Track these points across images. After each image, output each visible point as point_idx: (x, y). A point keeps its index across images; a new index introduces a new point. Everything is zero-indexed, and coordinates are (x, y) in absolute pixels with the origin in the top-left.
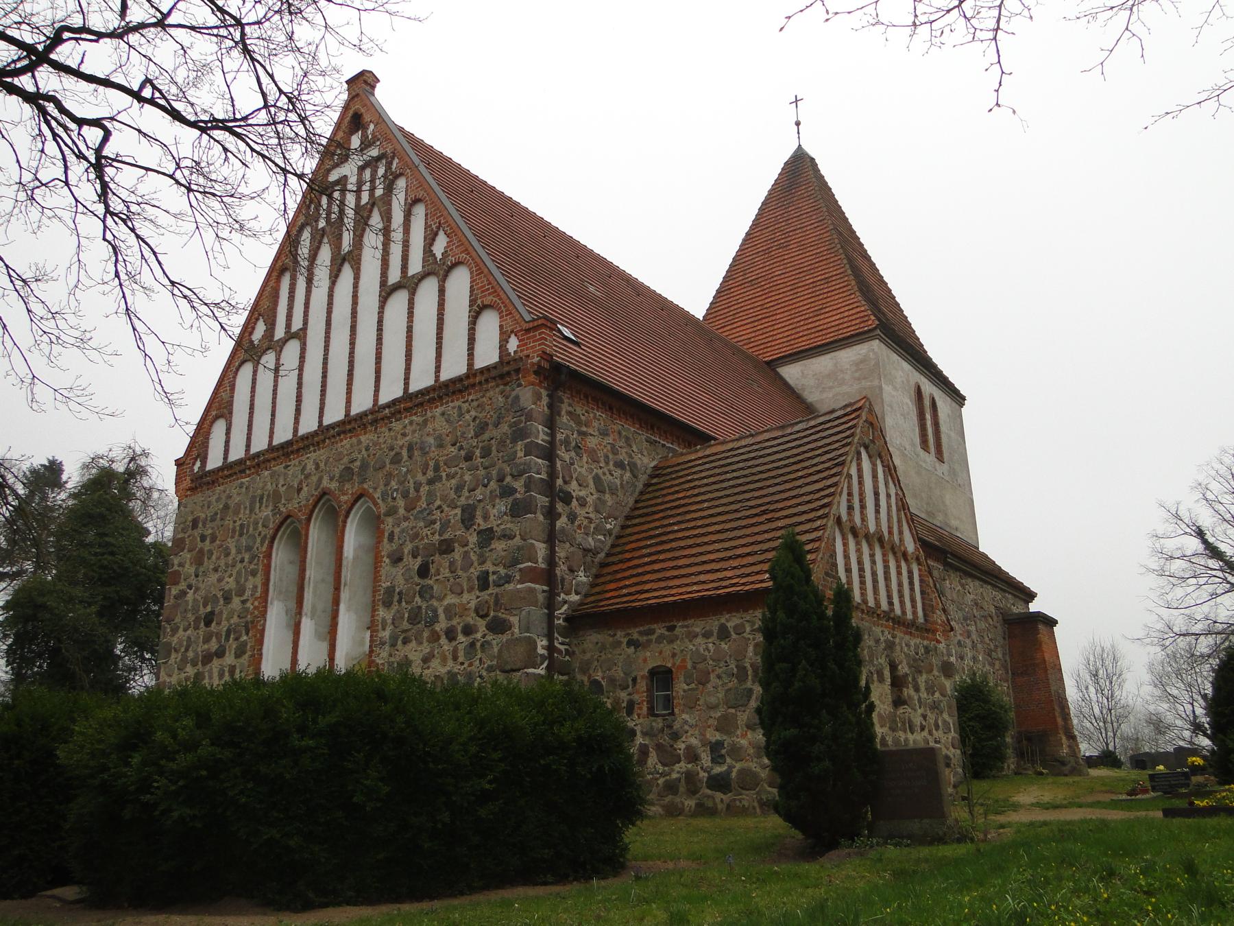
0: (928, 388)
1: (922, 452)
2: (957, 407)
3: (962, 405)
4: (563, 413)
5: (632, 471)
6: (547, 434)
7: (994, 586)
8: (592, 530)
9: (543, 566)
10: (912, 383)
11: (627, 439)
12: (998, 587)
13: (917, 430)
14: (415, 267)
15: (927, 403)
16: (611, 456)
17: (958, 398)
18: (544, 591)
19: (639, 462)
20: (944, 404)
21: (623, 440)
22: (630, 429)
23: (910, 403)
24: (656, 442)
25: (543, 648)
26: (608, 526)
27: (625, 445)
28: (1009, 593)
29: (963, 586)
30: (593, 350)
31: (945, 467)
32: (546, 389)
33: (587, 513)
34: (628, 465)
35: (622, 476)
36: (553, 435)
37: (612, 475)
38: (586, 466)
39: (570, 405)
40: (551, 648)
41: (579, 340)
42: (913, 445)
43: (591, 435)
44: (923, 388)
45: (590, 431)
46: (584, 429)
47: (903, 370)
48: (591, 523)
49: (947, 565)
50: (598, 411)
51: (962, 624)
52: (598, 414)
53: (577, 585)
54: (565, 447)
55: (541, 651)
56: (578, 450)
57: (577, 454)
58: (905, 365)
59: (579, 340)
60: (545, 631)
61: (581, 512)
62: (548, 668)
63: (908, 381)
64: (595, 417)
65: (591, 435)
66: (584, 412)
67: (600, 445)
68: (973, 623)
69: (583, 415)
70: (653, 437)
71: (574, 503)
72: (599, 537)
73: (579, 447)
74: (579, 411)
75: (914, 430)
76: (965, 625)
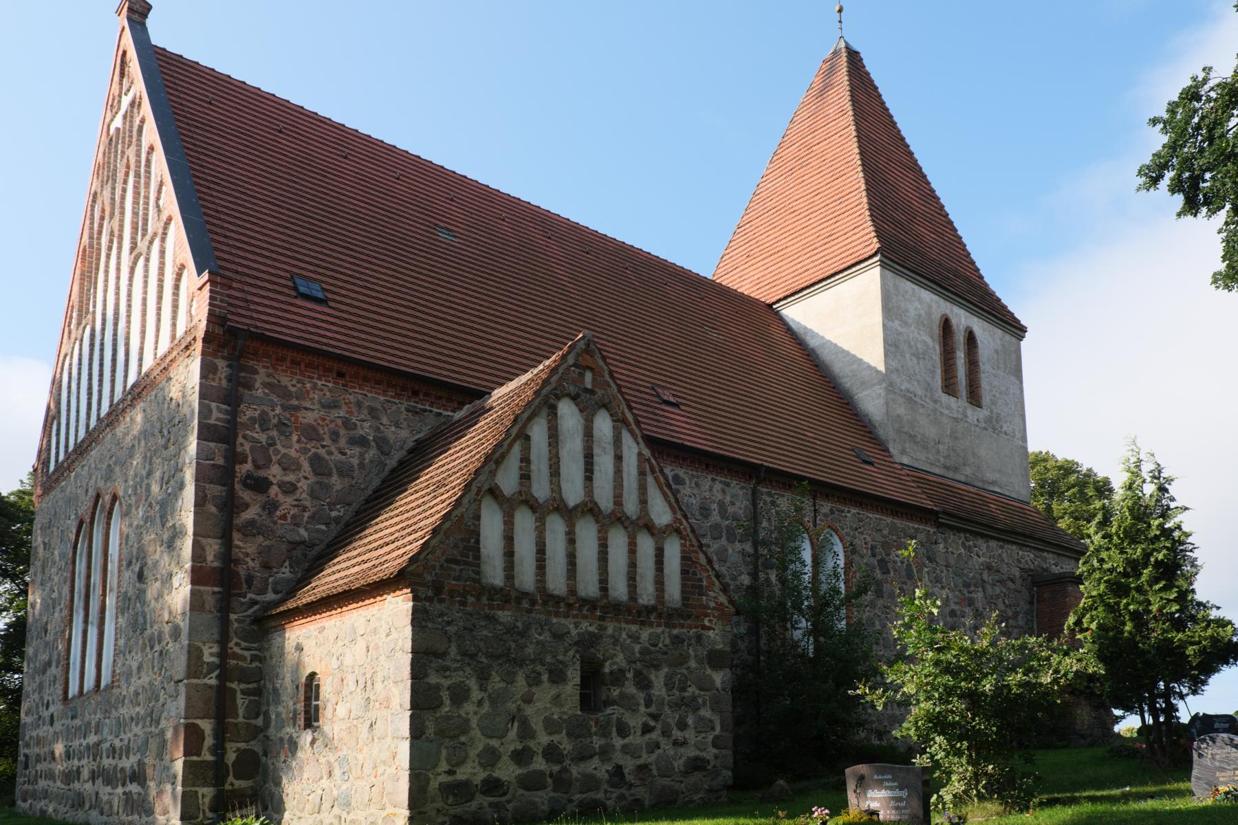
0: (962, 319)
1: (945, 398)
2: (1014, 340)
3: (1021, 338)
4: (257, 385)
5: (379, 448)
6: (226, 412)
7: (1021, 546)
8: (305, 519)
9: (216, 564)
10: (936, 317)
11: (372, 411)
12: (1027, 546)
13: (939, 372)
14: (290, 284)
15: (960, 338)
16: (342, 432)
17: (1017, 330)
18: (214, 593)
19: (391, 438)
20: (988, 336)
21: (366, 412)
22: (376, 398)
23: (929, 340)
24: (425, 411)
25: (211, 654)
26: (334, 514)
27: (368, 417)
28: (1048, 552)
29: (969, 549)
30: (729, 412)
31: (982, 413)
32: (223, 358)
33: (296, 500)
34: (374, 440)
35: (362, 455)
36: (234, 414)
37: (345, 454)
38: (297, 446)
39: (269, 376)
40: (223, 654)
41: (679, 400)
42: (928, 388)
43: (306, 409)
44: (954, 321)
45: (308, 404)
46: (294, 402)
47: (920, 300)
48: (304, 511)
49: (939, 525)
50: (319, 379)
51: (960, 591)
52: (319, 383)
53: (275, 583)
54: (260, 426)
55: (207, 658)
56: (283, 428)
57: (281, 433)
58: (926, 295)
59: (679, 400)
60: (216, 637)
61: (287, 502)
62: (218, 677)
63: (929, 314)
64: (315, 387)
65: (306, 409)
66: (294, 382)
67: (323, 420)
68: (980, 589)
69: (293, 386)
70: (419, 406)
71: (274, 490)
72: (305, 519)
73: (285, 424)
74: (285, 380)
75: (933, 372)
76: (965, 592)
